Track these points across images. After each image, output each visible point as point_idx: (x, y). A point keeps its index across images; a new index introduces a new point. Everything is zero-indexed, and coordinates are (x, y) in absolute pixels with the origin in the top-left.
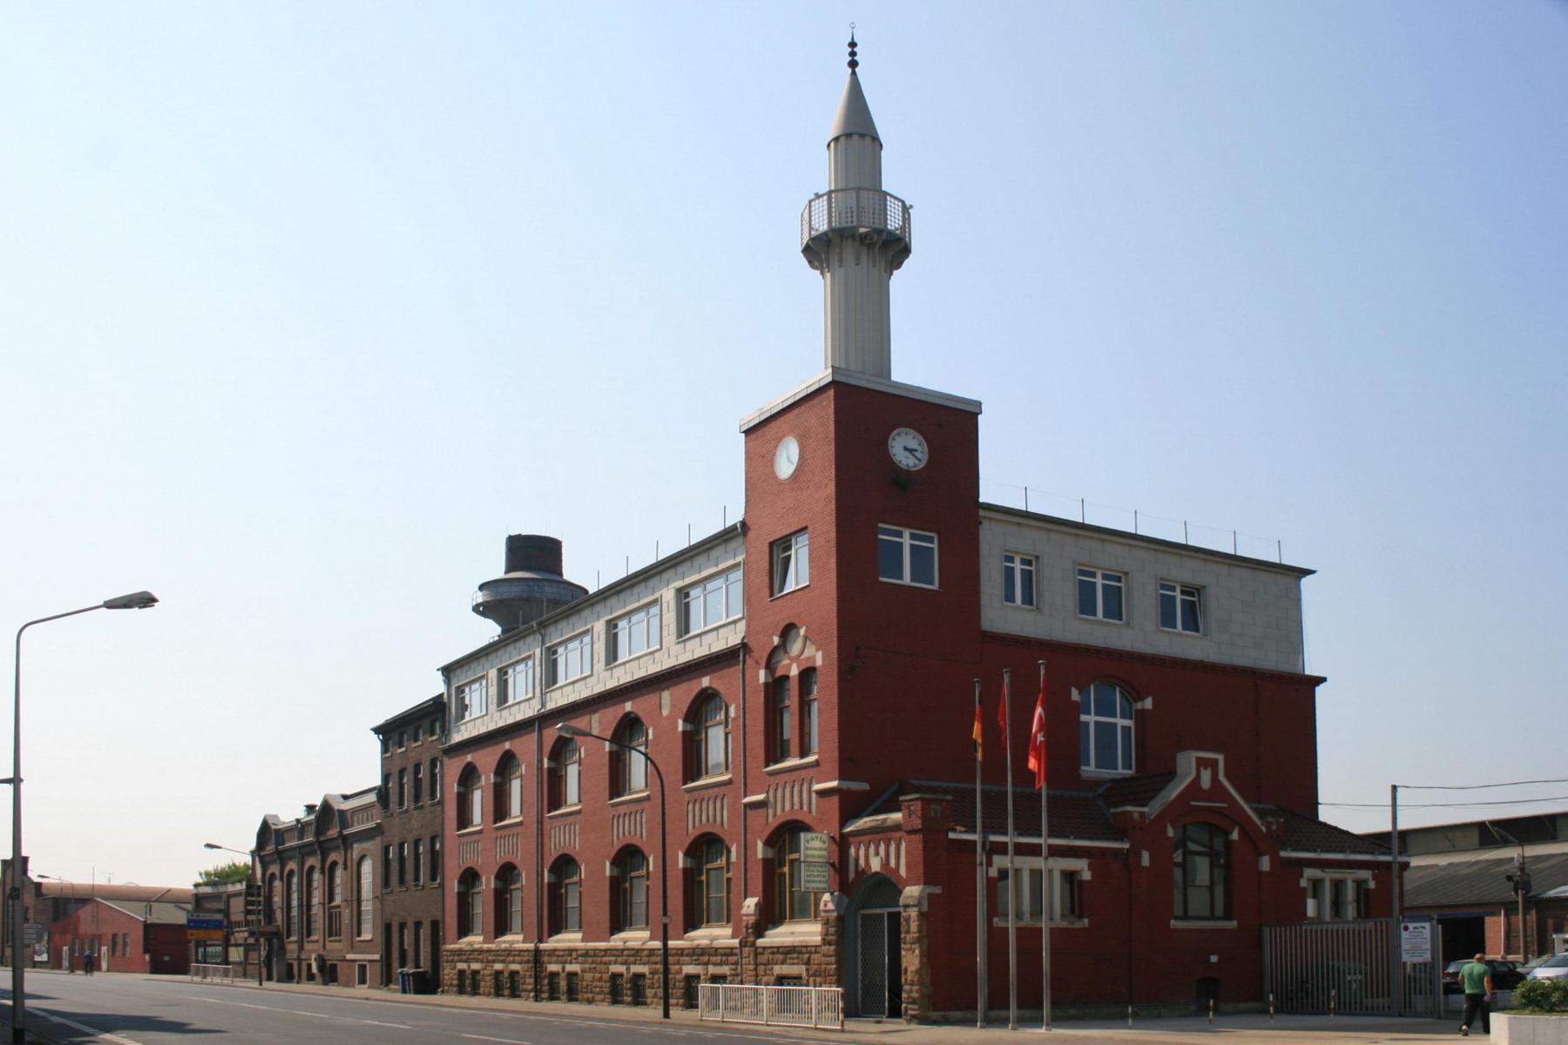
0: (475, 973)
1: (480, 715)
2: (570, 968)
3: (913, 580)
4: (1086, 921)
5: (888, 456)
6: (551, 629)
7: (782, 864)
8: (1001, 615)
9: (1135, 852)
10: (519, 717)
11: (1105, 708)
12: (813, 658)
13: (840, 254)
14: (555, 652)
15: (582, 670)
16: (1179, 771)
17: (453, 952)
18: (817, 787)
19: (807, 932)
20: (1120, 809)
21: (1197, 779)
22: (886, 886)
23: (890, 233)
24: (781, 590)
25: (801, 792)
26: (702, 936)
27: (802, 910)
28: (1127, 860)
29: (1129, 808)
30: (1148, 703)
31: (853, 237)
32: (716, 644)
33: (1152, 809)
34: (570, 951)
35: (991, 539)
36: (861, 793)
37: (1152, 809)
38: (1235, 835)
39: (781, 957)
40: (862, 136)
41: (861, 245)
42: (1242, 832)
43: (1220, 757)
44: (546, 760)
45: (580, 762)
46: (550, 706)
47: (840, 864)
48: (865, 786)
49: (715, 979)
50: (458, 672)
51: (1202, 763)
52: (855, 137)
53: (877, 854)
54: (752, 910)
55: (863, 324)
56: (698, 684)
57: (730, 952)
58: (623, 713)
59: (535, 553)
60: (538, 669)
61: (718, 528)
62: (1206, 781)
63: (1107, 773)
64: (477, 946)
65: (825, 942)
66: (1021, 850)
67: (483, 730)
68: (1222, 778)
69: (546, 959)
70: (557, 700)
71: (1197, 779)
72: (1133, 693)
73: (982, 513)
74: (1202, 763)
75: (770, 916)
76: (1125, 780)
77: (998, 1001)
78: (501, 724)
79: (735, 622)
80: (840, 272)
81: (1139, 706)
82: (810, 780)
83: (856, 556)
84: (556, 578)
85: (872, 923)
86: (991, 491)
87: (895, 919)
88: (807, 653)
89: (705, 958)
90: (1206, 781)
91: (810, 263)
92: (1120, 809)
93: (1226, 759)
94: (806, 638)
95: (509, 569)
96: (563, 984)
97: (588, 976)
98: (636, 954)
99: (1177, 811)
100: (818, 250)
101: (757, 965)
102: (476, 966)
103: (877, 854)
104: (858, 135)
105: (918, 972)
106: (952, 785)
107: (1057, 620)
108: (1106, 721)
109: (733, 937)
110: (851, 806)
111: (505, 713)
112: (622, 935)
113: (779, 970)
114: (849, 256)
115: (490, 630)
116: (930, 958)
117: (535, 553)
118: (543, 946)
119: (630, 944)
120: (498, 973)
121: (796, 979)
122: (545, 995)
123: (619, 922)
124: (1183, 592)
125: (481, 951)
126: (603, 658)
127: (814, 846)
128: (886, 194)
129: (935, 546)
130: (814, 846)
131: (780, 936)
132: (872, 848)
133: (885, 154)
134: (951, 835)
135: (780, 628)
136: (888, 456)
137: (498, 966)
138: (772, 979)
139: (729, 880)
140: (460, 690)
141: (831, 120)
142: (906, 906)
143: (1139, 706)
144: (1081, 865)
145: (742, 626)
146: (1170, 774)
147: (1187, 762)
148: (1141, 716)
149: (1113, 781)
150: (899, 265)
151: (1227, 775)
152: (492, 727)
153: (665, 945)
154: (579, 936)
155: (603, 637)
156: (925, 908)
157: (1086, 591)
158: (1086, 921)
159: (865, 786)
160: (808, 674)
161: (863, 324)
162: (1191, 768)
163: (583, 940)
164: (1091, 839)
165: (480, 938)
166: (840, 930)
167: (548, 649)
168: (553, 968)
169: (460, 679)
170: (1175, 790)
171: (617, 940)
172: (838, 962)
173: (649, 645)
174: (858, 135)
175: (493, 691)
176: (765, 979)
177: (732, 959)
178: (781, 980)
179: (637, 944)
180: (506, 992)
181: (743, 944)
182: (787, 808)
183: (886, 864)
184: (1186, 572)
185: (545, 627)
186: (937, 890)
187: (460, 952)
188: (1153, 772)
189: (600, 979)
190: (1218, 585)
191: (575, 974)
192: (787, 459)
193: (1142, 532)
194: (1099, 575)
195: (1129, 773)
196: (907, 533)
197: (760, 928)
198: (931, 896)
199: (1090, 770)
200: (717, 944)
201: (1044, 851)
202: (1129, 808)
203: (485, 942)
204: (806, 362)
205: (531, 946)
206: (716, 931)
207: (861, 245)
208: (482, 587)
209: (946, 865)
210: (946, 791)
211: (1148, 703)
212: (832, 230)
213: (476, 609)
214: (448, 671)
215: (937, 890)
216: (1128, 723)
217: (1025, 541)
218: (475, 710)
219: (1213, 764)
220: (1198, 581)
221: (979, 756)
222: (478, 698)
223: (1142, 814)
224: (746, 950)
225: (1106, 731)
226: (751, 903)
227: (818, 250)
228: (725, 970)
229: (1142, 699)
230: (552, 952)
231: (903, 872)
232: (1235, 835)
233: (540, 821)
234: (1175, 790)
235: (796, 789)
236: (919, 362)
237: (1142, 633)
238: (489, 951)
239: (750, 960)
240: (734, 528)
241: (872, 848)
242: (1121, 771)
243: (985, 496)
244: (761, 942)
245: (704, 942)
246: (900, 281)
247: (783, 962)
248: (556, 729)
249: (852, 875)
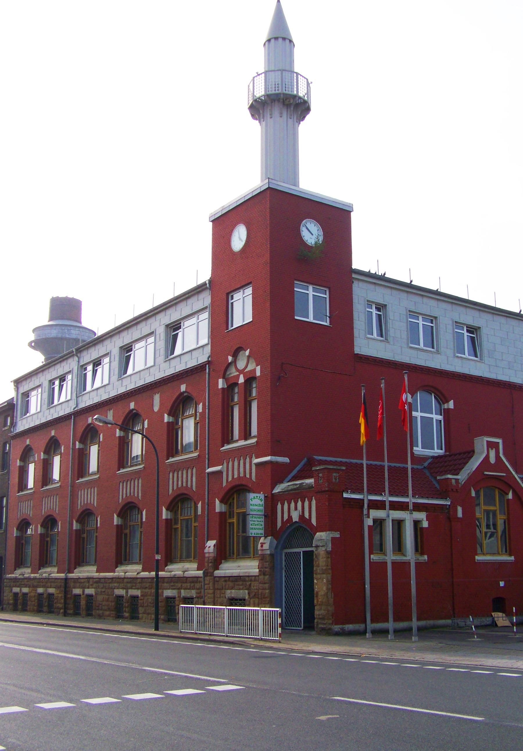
0: (25, 594)
1: (37, 412)
2: (88, 591)
3: (314, 319)
4: (426, 557)
5: (287, 241)
6: (84, 353)
7: (176, 523)
8: (367, 344)
9: (453, 507)
10: (61, 414)
11: (426, 408)
12: (254, 371)
13: (271, 110)
14: (86, 369)
15: (103, 383)
16: (476, 451)
17: (10, 579)
18: (256, 461)
19: (250, 567)
20: (443, 477)
21: (487, 456)
22: (302, 531)
23: (300, 98)
24: (232, 326)
25: (53, 499)
26: (176, 569)
27: (246, 549)
28: (448, 512)
29: (450, 476)
30: (451, 405)
31: (279, 100)
32: (191, 363)
33: (463, 476)
34: (89, 579)
35: (360, 293)
36: (283, 464)
37: (463, 476)
38: (510, 496)
39: (231, 584)
40: (284, 39)
41: (282, 105)
42: (515, 493)
43: (500, 441)
44: (77, 443)
45: (61, 454)
46: (82, 405)
47: (270, 515)
48: (286, 460)
49: (188, 600)
50: (24, 383)
51: (490, 445)
52: (280, 40)
53: (296, 509)
54: (212, 549)
55: (282, 153)
56: (178, 390)
57: (195, 579)
58: (128, 408)
59: (66, 309)
60: (75, 381)
61: (193, 285)
62: (492, 460)
63: (428, 452)
64: (26, 575)
65: (262, 572)
66: (395, 506)
67: (38, 423)
68: (501, 455)
69: (72, 584)
70: (86, 402)
71: (487, 456)
72: (442, 399)
73: (354, 276)
74: (490, 445)
75: (223, 554)
76: (440, 457)
77: (380, 615)
78: (50, 418)
79: (203, 346)
80: (270, 121)
81: (446, 406)
82: (245, 458)
83: (277, 304)
84: (78, 325)
85: (292, 558)
86: (359, 262)
87: (309, 557)
88: (248, 369)
89: (179, 585)
90: (492, 460)
91: (252, 116)
92: (443, 477)
93: (504, 442)
94: (249, 357)
95: (51, 319)
96: (83, 603)
97: (100, 598)
98: (133, 582)
99: (478, 478)
100: (258, 108)
101: (214, 589)
102: (25, 590)
103: (296, 509)
104: (280, 38)
105: (326, 594)
106: (344, 460)
107: (395, 348)
108: (426, 415)
109: (198, 569)
110: (278, 473)
111: (52, 410)
112: (124, 568)
113: (230, 593)
114: (276, 112)
115: (38, 359)
116: (335, 585)
117: (66, 309)
118: (71, 575)
119: (129, 574)
120: (41, 595)
121: (241, 602)
122: (71, 612)
123: (122, 558)
124: (468, 331)
125: (29, 579)
126: (117, 372)
127: (255, 502)
128: (297, 74)
129: (327, 296)
130: (255, 502)
131: (230, 568)
132: (293, 505)
133: (297, 51)
134: (345, 495)
135: (233, 351)
136: (287, 241)
137: (40, 590)
138: (225, 600)
139: (96, 536)
140: (26, 395)
141: (264, 31)
142: (317, 547)
143: (446, 406)
144: (422, 516)
145: (208, 349)
146: (470, 453)
147: (481, 443)
148: (446, 413)
149: (433, 457)
150: (303, 119)
151: (504, 454)
152: (43, 420)
153: (157, 575)
154: (94, 568)
155: (117, 359)
156: (329, 549)
157: (413, 328)
158: (426, 557)
159: (286, 460)
160: (250, 379)
161: (282, 153)
162: (485, 449)
163: (98, 571)
164: (428, 498)
165: (29, 570)
166: (269, 564)
167: (82, 366)
168: (77, 591)
169: (25, 387)
170: (474, 464)
171: (120, 572)
172: (271, 588)
173: (147, 362)
174: (280, 38)
175: (46, 395)
176: (220, 600)
177: (198, 585)
178: (233, 601)
179: (133, 574)
180: (45, 609)
181: (205, 574)
182: (180, 485)
183: (302, 517)
184: (470, 318)
185: (81, 352)
186: (337, 535)
187: (15, 579)
188: (457, 454)
189: (107, 600)
190: (487, 325)
191: (91, 596)
192: (239, 238)
193: (443, 290)
194: (420, 318)
195: (441, 452)
196: (311, 288)
197: (217, 563)
198: (333, 539)
199: (418, 450)
200: (187, 574)
201: (411, 507)
202: (450, 476)
203: (32, 572)
204: (246, 179)
205: (62, 575)
206: (187, 565)
207: (282, 105)
208: (34, 331)
209: (344, 516)
210: (341, 464)
211: (451, 405)
212: (267, 96)
213: (30, 344)
214: (18, 382)
215: (337, 535)
216: (440, 418)
217: (380, 295)
218: (33, 409)
219: (494, 446)
220: (476, 324)
221: (363, 439)
222: (35, 402)
223: (457, 480)
224: (208, 578)
225: (427, 422)
226: (211, 544)
227: (258, 108)
228: (193, 593)
229: (447, 401)
230: (77, 580)
231: (314, 521)
232: (510, 496)
233: (73, 485)
234: (474, 464)
235: (125, 484)
236: (314, 180)
237: (448, 359)
238: (35, 579)
239: (211, 588)
240: (205, 284)
241: (293, 505)
242: (437, 452)
243: (356, 265)
244: (217, 573)
245: (179, 573)
246: (306, 128)
247: (232, 588)
248: (82, 425)
249: (279, 524)
